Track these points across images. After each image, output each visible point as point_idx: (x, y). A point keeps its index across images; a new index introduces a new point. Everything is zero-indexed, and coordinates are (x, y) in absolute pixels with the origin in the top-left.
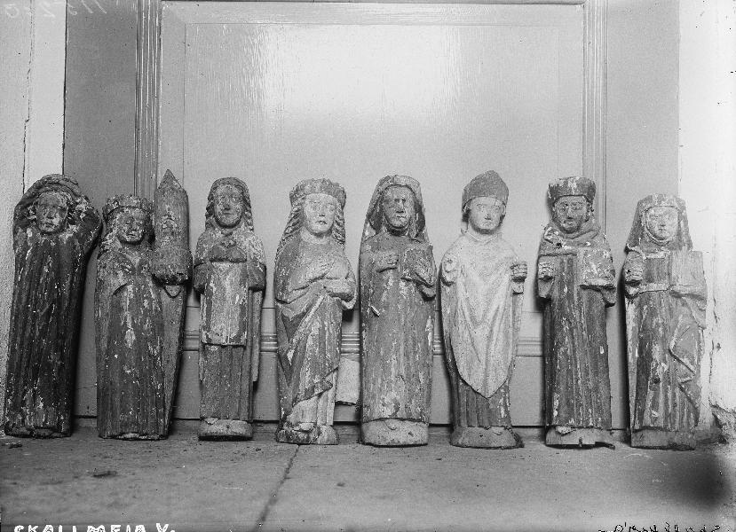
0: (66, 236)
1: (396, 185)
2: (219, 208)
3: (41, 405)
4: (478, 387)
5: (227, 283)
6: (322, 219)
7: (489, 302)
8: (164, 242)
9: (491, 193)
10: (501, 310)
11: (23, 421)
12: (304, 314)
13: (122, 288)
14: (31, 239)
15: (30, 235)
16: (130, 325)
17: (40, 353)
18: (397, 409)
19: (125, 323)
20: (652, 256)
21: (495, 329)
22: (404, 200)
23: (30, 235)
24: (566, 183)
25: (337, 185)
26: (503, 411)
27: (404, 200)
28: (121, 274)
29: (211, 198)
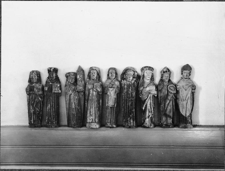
0: (133, 81)
1: (93, 69)
2: (110, 75)
3: (132, 121)
4: (184, 115)
5: (112, 93)
6: (149, 76)
7: (187, 95)
8: (79, 83)
9: (187, 70)
10: (189, 97)
11: (128, 125)
12: (146, 99)
13: (71, 94)
14: (126, 83)
15: (125, 82)
16: (73, 102)
17: (131, 109)
18: (93, 120)
19: (72, 102)
20: (32, 85)
21: (188, 101)
22: (94, 73)
23: (125, 82)
24: (50, 69)
25: (81, 70)
26: (190, 120)
27: (94, 73)
28: (71, 91)
29: (108, 72)
